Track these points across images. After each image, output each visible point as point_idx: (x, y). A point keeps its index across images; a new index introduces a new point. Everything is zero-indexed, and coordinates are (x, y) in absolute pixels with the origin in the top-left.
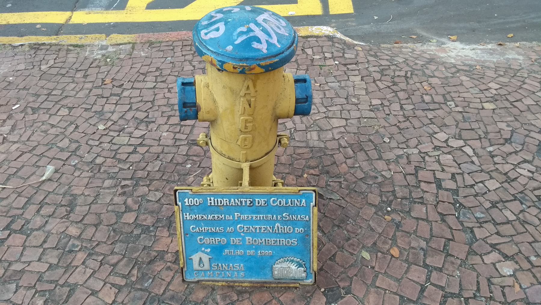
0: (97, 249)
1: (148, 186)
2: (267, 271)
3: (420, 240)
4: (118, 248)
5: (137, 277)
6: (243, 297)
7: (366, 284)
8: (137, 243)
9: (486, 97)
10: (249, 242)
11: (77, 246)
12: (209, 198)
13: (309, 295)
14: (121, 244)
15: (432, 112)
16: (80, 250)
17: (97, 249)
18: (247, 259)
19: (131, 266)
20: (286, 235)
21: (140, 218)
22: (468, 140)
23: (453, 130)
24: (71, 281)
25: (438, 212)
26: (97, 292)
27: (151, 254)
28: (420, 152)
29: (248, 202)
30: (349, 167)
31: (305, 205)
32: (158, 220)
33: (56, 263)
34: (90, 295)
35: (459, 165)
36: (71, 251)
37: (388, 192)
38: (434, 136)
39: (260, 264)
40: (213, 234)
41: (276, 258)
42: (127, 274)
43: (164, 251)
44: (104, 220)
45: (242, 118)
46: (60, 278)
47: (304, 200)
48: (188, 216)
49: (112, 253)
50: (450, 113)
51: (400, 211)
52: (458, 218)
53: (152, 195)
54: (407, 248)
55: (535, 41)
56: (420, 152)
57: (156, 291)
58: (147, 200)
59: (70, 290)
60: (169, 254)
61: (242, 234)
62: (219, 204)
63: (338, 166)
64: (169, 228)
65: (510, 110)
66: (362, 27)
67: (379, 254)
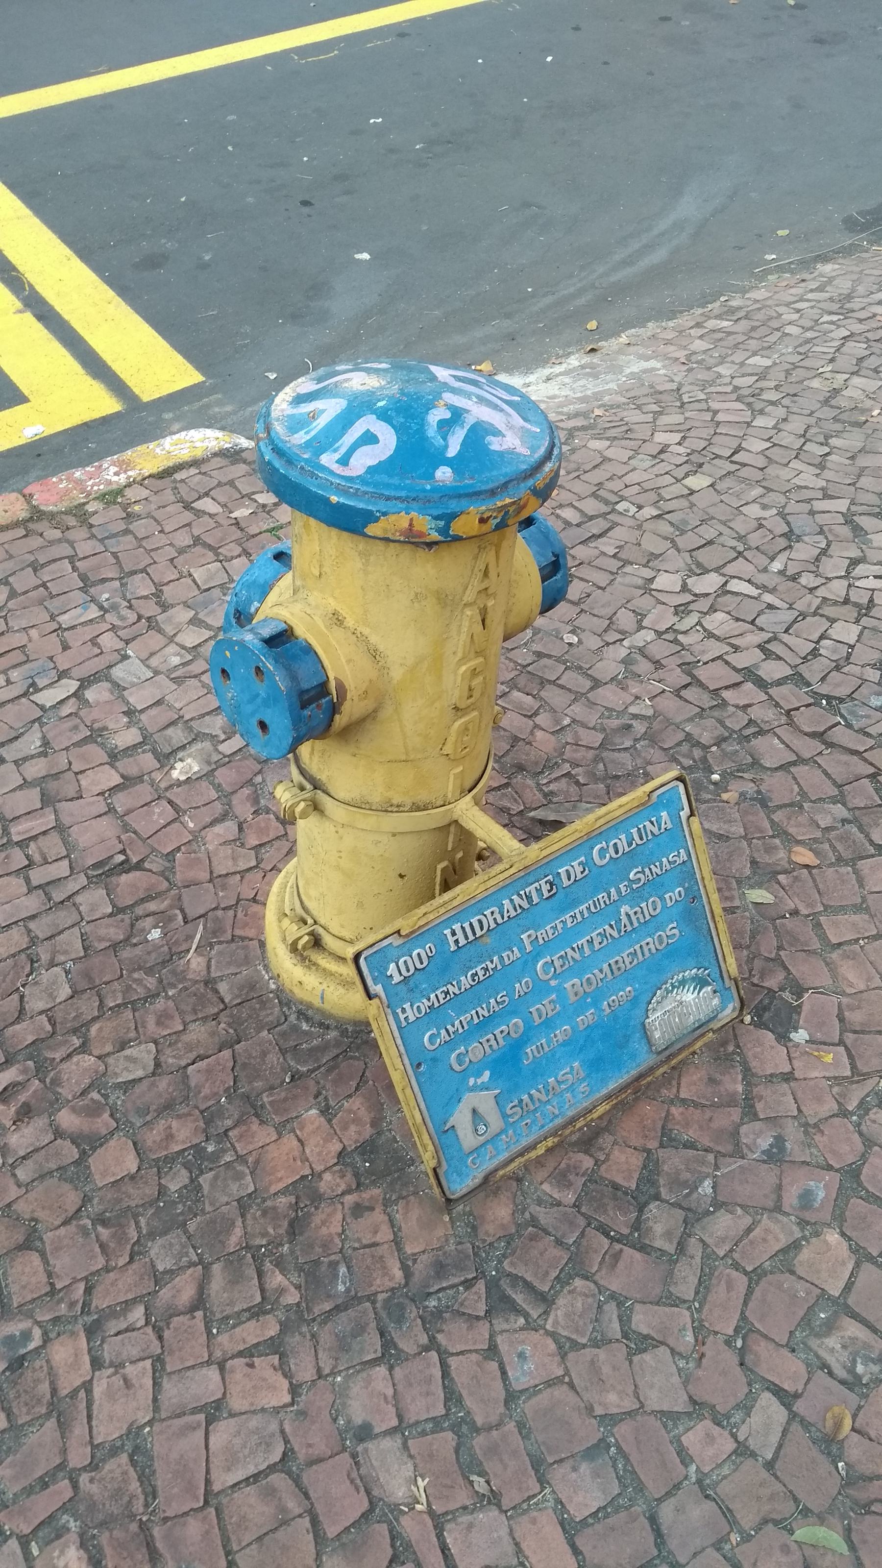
0: (100, 1301)
1: (84, 1048)
2: (637, 1045)
3: (826, 806)
4: (161, 1254)
5: (298, 1287)
6: (601, 1149)
8: (208, 1208)
9: (677, 466)
11: (26, 1336)
12: (447, 932)
13: (731, 1048)
14: (160, 1241)
15: (604, 539)
17: (100, 1301)
19: (251, 1272)
20: (650, 924)
21: (149, 1143)
23: (679, 561)
24: (107, 1431)
25: (805, 734)
26: (218, 1404)
27: (274, 1208)
28: (659, 634)
31: (669, 826)
32: (210, 1117)
34: (208, 1423)
35: (753, 622)
37: (679, 744)
38: (653, 587)
39: (614, 1035)
40: (485, 1024)
41: (645, 998)
42: (258, 1299)
43: (303, 1178)
44: (40, 1214)
45: (464, 668)
46: (64, 1451)
47: (664, 814)
49: (159, 1279)
50: (640, 527)
51: (738, 771)
52: (849, 726)
53: (122, 1063)
54: (818, 834)
56: (659, 634)
57: (381, 1283)
58: (118, 1086)
59: (131, 1457)
60: (327, 1176)
61: (553, 983)
62: (479, 933)
63: (530, 743)
64: (257, 1115)
65: (739, 473)
67: (781, 877)
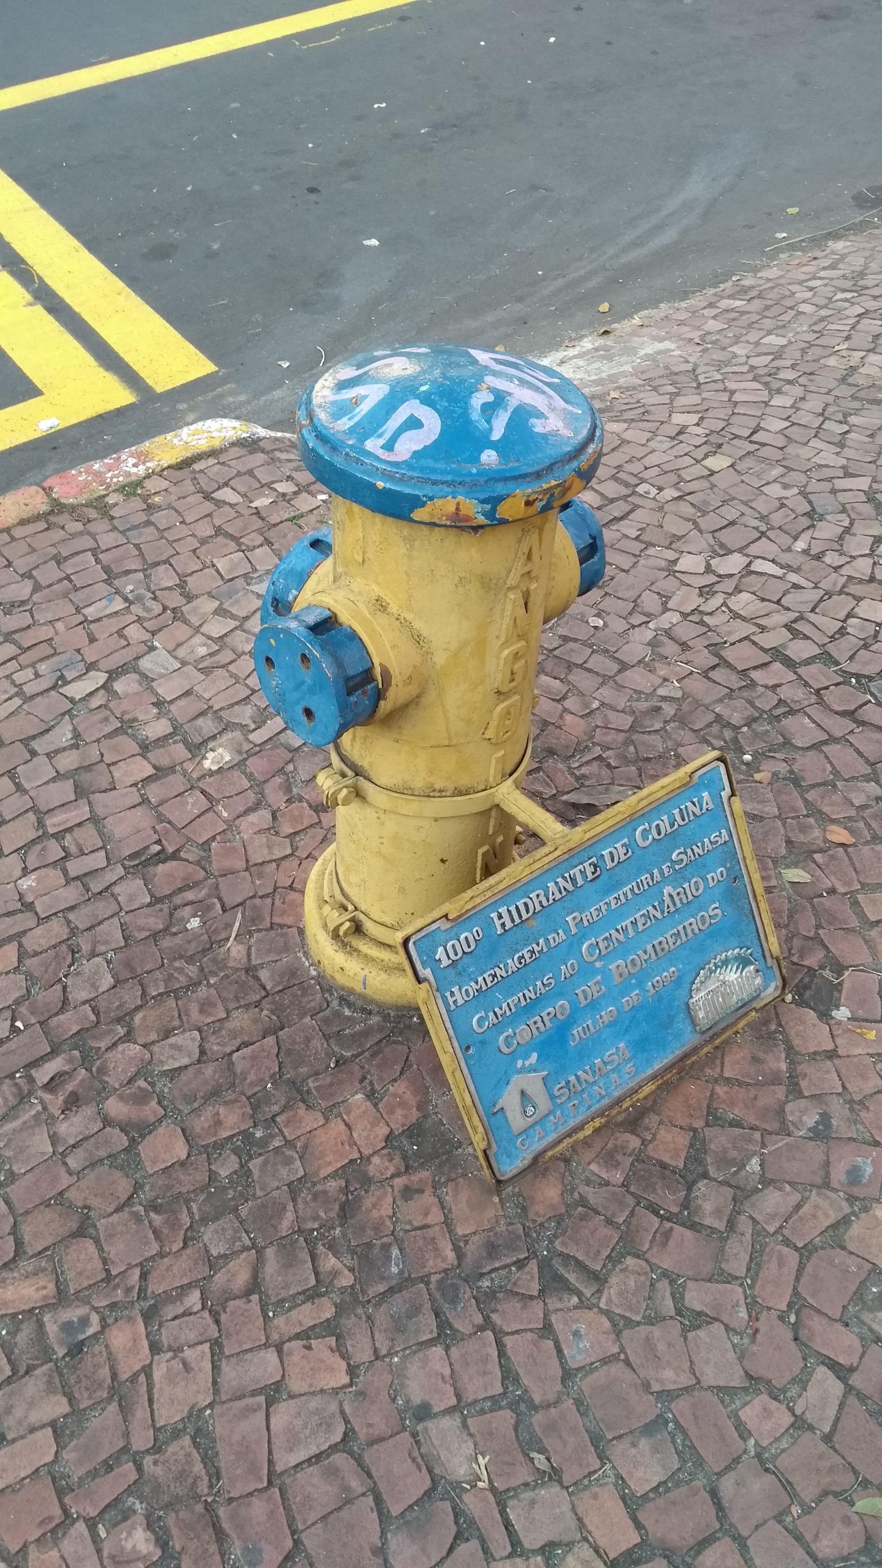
0: (156, 1287)
1: (129, 1037)
2: (682, 1024)
3: (859, 784)
5: (351, 1270)
7: (853, 930)
8: (259, 1193)
9: (696, 447)
10: (621, 975)
11: (84, 1322)
12: (494, 915)
13: (773, 1027)
14: (212, 1227)
16: (104, 1325)
17: (156, 1287)
18: (627, 1023)
19: (305, 1256)
21: (198, 1130)
22: (34, 737)
23: (702, 542)
25: (836, 713)
26: (278, 1386)
27: (325, 1192)
28: (685, 615)
29: (589, 870)
30: (582, 717)
31: (711, 806)
32: (256, 1103)
33: (66, 1409)
34: (269, 1404)
35: (778, 602)
36: (76, 1350)
37: (709, 725)
39: (661, 1013)
40: (532, 1006)
41: (688, 979)
42: (313, 1282)
43: (352, 1161)
44: (93, 1202)
46: (127, 1434)
47: (705, 794)
48: (458, 995)
49: (213, 1263)
50: (661, 509)
51: (770, 751)
54: (853, 813)
55: (662, 302)
56: (685, 615)
58: (165, 1073)
59: (193, 1439)
60: (376, 1160)
61: (598, 965)
62: (525, 916)
63: (560, 727)
64: (303, 1101)
65: (759, 453)
66: (269, 397)
67: (817, 857)
